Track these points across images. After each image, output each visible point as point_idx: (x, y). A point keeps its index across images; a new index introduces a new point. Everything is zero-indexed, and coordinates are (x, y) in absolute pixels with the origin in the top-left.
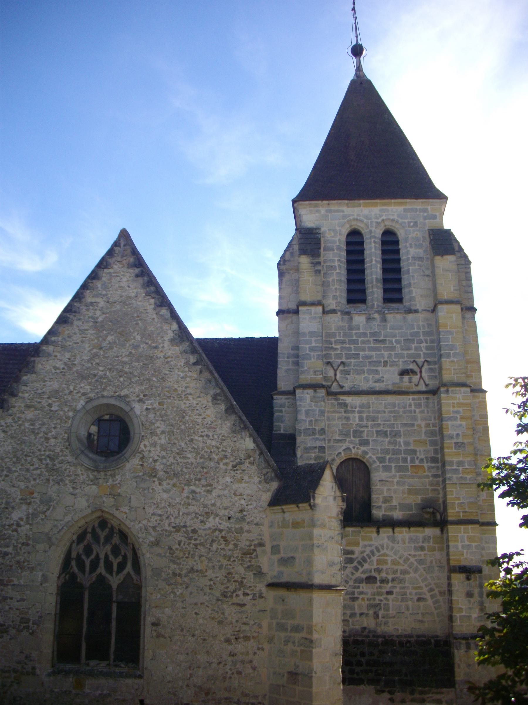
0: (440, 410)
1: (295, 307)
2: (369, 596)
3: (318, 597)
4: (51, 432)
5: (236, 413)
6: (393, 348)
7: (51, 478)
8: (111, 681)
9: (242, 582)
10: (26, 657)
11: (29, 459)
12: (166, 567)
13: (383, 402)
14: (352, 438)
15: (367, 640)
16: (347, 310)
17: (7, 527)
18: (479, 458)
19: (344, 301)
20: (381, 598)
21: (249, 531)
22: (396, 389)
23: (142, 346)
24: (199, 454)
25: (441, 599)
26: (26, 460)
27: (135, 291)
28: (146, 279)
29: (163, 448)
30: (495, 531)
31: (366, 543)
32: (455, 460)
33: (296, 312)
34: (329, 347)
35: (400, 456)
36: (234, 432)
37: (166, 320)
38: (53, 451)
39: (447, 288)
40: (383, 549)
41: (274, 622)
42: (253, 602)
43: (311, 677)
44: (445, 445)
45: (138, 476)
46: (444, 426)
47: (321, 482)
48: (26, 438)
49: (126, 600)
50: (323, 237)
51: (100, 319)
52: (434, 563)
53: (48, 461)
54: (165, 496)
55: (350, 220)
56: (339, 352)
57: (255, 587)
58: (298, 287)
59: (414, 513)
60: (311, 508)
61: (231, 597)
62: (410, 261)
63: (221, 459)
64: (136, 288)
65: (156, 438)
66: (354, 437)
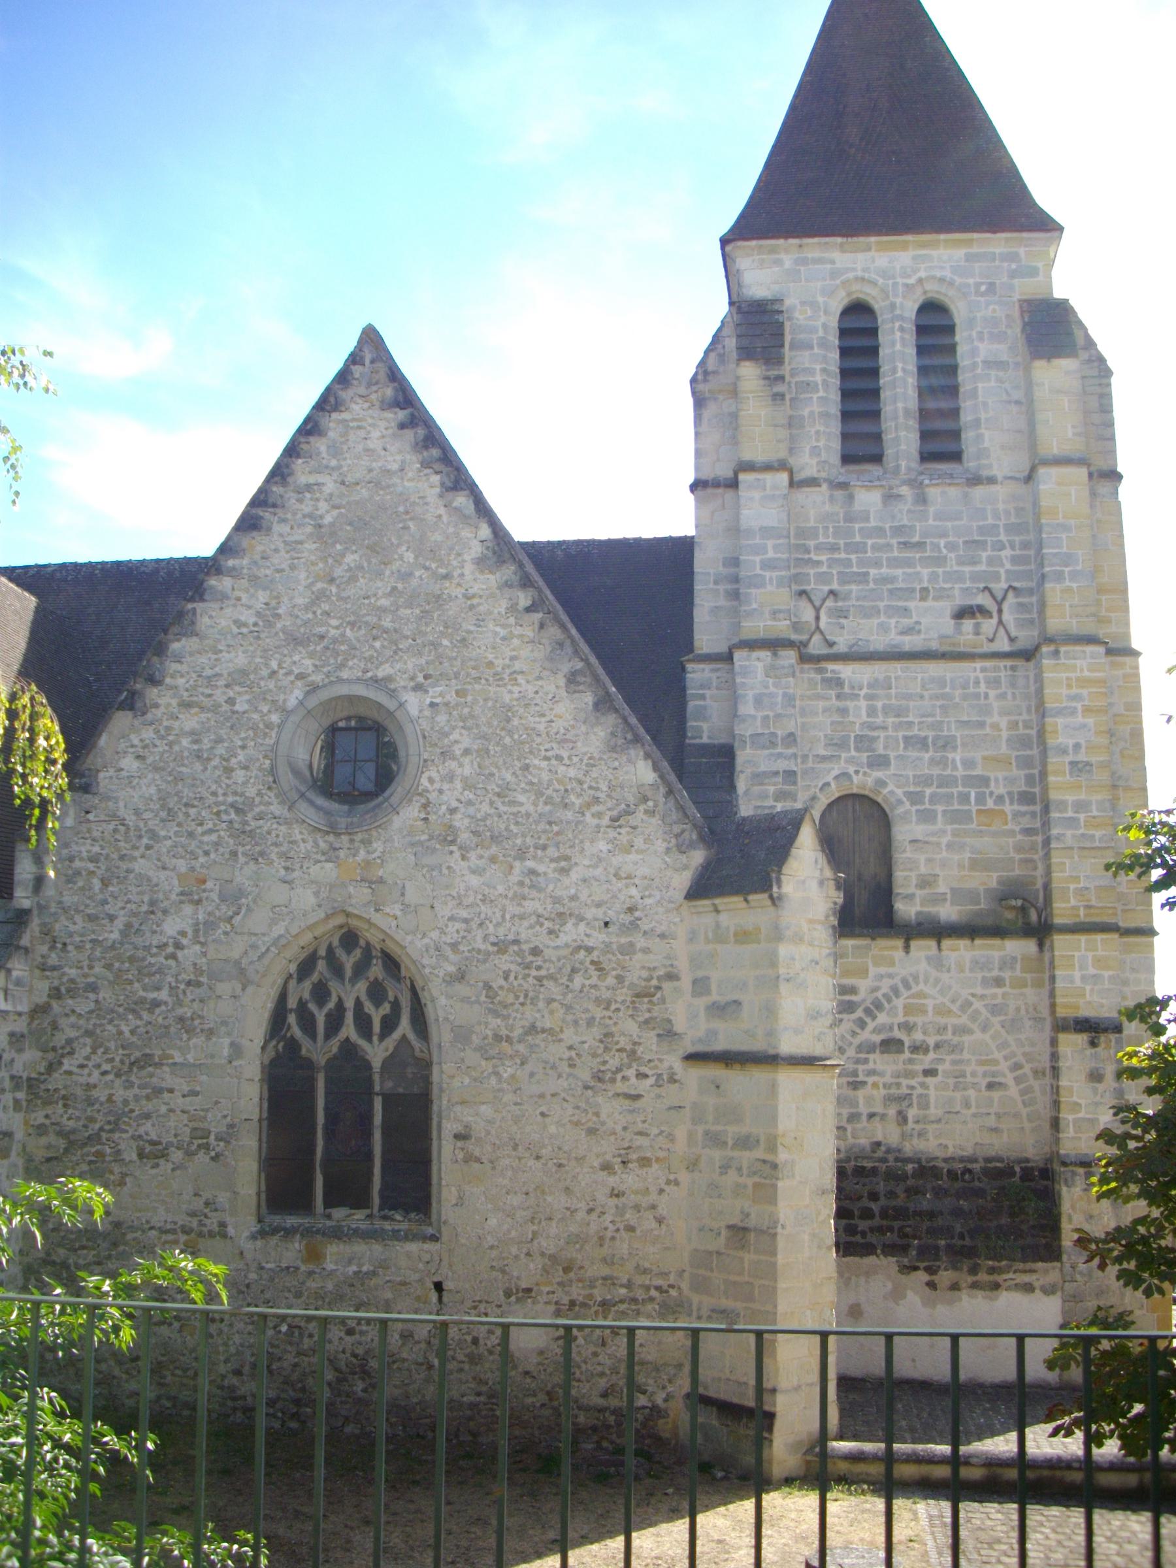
0: (1040, 692)
1: (730, 474)
2: (888, 1079)
3: (788, 1080)
4: (235, 755)
5: (616, 711)
6: (941, 561)
7: (240, 849)
8: (377, 1248)
9: (634, 1052)
10: (207, 1204)
11: (192, 812)
12: (479, 1023)
13: (920, 676)
14: (853, 753)
15: (883, 1167)
16: (842, 479)
17: (155, 950)
19: (836, 459)
20: (913, 1082)
21: (646, 951)
23: (417, 574)
24: (542, 794)
25: (1036, 1085)
26: (187, 815)
27: (399, 458)
28: (421, 432)
29: (468, 785)
30: (1151, 945)
31: (883, 970)
32: (1070, 798)
33: (733, 484)
35: (955, 790)
36: (613, 749)
37: (465, 518)
38: (242, 795)
39: (1060, 430)
40: (917, 984)
41: (700, 1129)
42: (657, 1090)
43: (775, 1234)
44: (1050, 768)
45: (421, 843)
46: (1048, 728)
47: (794, 851)
48: (184, 769)
49: (401, 1090)
50: (789, 319)
51: (328, 519)
52: (1023, 1012)
53: (233, 816)
54: (474, 881)
56: (824, 569)
57: (661, 1060)
58: (736, 429)
60: (774, 904)
61: (613, 1080)
62: (979, 371)
63: (588, 805)
64: (400, 452)
65: (453, 765)
66: (857, 749)
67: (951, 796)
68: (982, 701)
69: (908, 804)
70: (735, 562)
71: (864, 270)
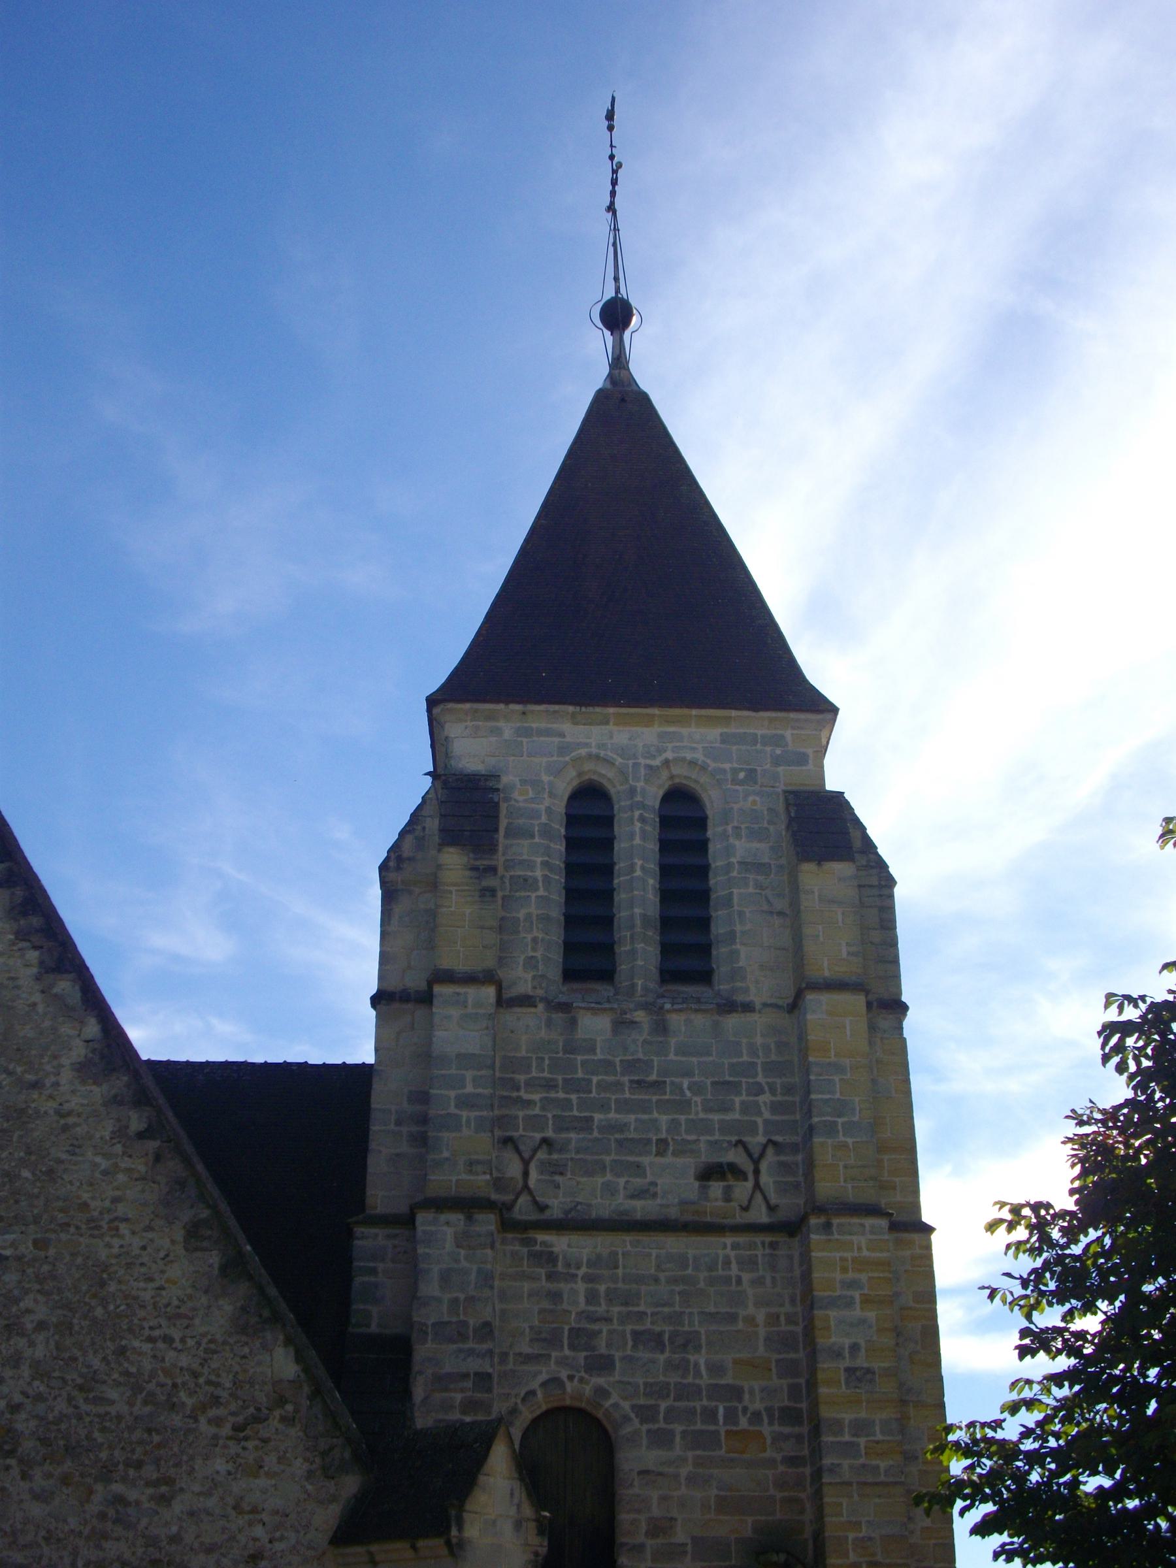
0: (807, 1276)
1: (423, 986)
6: (683, 1105)
13: (654, 1252)
14: (567, 1352)
16: (563, 999)
19: (555, 973)
22: (688, 1217)
28: (19, 893)
29: (40, 1372)
32: (847, 1417)
33: (426, 998)
39: (832, 948)
44: (820, 1376)
46: (818, 1324)
47: (482, 1479)
50: (507, 799)
54: (37, 1510)
56: (537, 1111)
60: (452, 1553)
62: (735, 874)
63: (204, 1408)
65: (22, 1342)
66: (572, 1347)
67: (692, 1411)
68: (733, 1288)
69: (636, 1421)
70: (422, 1097)
71: (599, 746)
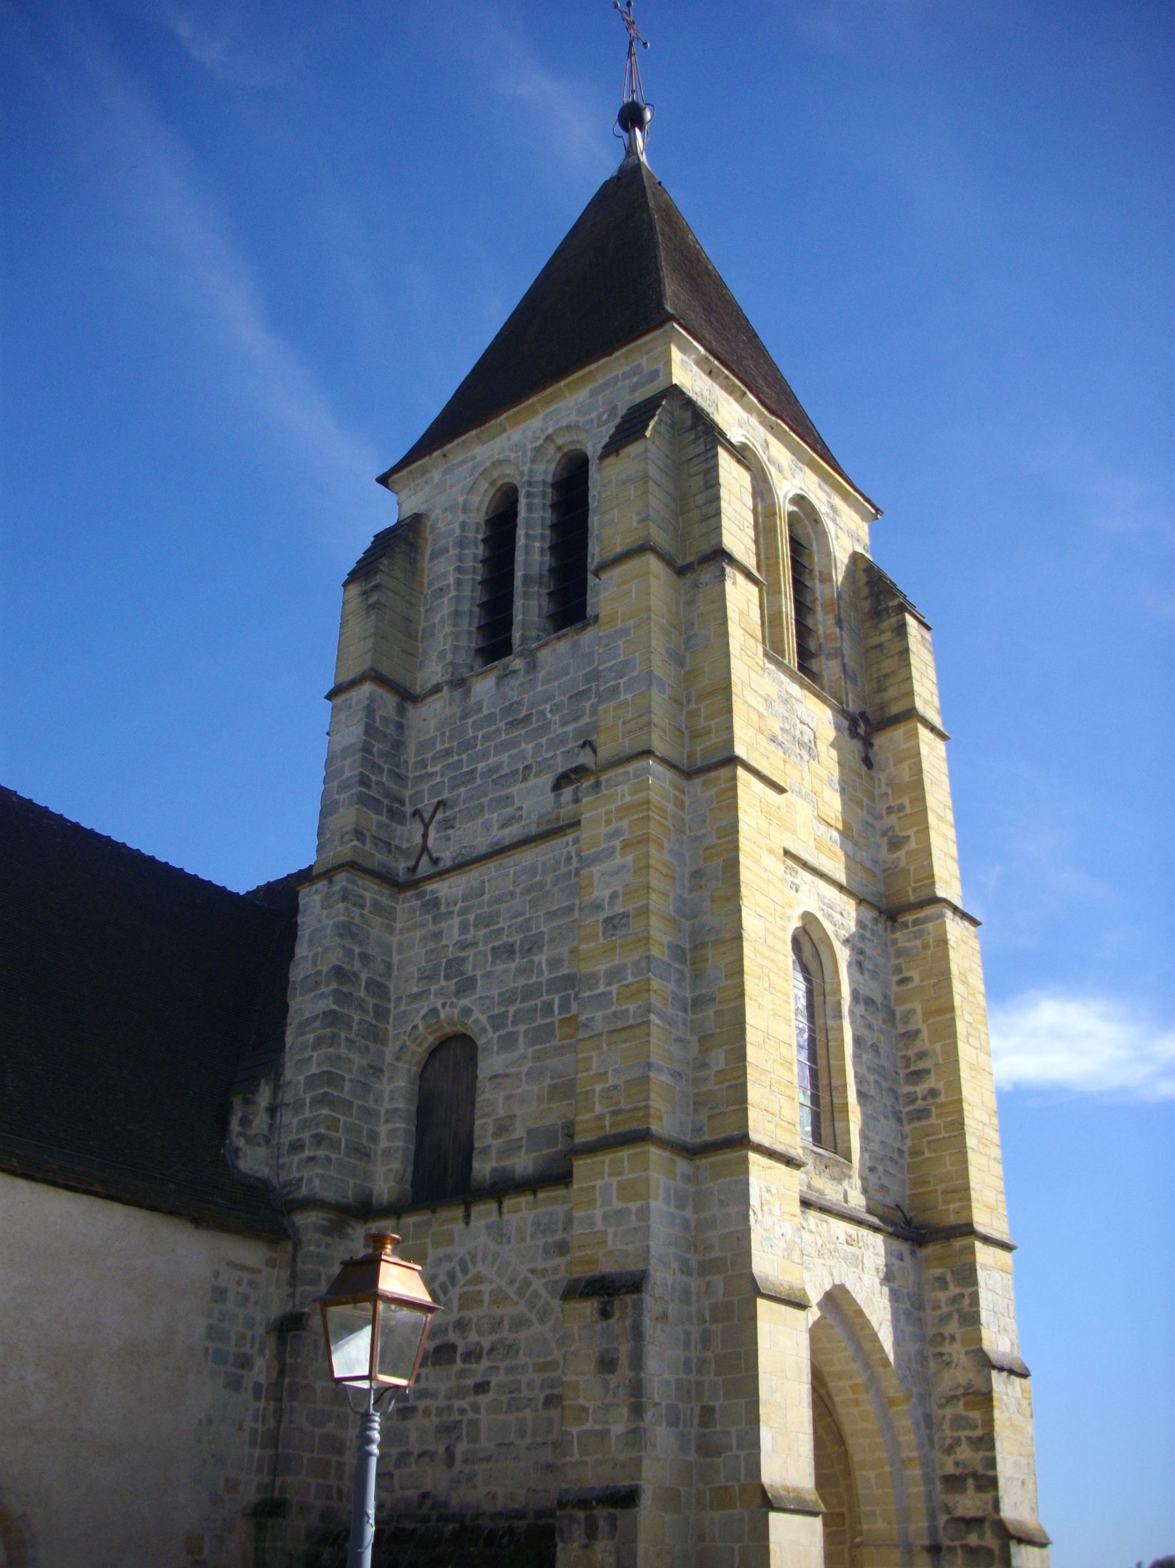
2: (441, 1402)
14: (443, 982)
18: (710, 954)
20: (464, 1404)
22: (544, 828)
31: (441, 1251)
32: (602, 967)
34: (421, 776)
35: (538, 1002)
55: (486, 470)
59: (560, 1151)
66: (447, 978)
